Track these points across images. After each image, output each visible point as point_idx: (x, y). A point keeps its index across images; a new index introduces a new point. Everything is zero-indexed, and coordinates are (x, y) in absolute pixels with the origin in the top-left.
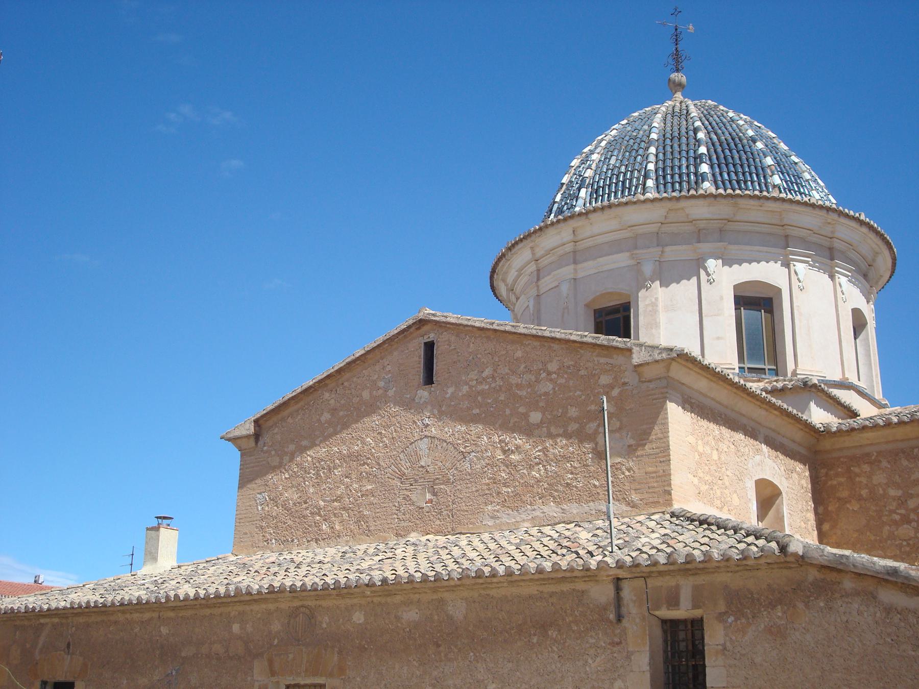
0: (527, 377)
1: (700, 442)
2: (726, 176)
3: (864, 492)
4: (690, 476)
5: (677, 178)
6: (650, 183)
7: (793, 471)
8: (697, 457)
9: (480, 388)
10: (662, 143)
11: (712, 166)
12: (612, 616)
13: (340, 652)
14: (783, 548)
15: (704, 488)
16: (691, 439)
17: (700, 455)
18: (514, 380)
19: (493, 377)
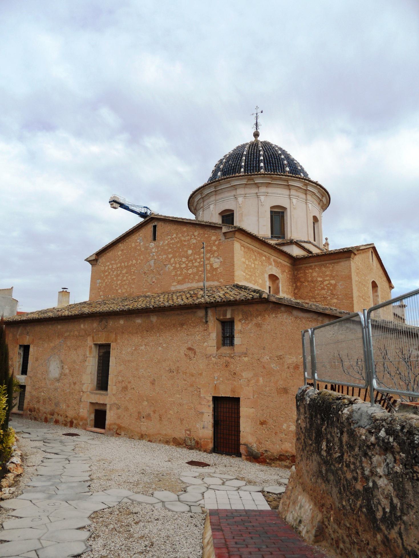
0: (187, 238)
1: (247, 261)
2: (269, 168)
3: (310, 279)
4: (242, 273)
5: (252, 168)
6: (242, 170)
7: (284, 271)
8: (245, 266)
9: (171, 242)
10: (247, 156)
11: (264, 164)
12: (204, 321)
13: (115, 334)
14: (260, 296)
15: (248, 277)
16: (243, 260)
17: (247, 265)
18: (183, 238)
19: (176, 238)
